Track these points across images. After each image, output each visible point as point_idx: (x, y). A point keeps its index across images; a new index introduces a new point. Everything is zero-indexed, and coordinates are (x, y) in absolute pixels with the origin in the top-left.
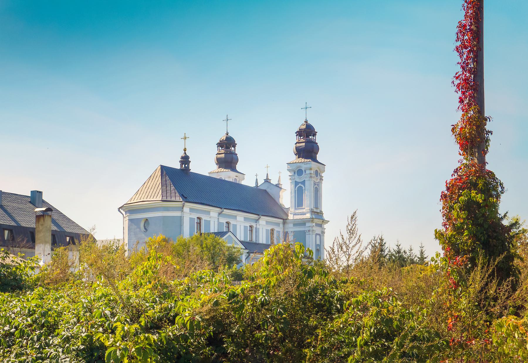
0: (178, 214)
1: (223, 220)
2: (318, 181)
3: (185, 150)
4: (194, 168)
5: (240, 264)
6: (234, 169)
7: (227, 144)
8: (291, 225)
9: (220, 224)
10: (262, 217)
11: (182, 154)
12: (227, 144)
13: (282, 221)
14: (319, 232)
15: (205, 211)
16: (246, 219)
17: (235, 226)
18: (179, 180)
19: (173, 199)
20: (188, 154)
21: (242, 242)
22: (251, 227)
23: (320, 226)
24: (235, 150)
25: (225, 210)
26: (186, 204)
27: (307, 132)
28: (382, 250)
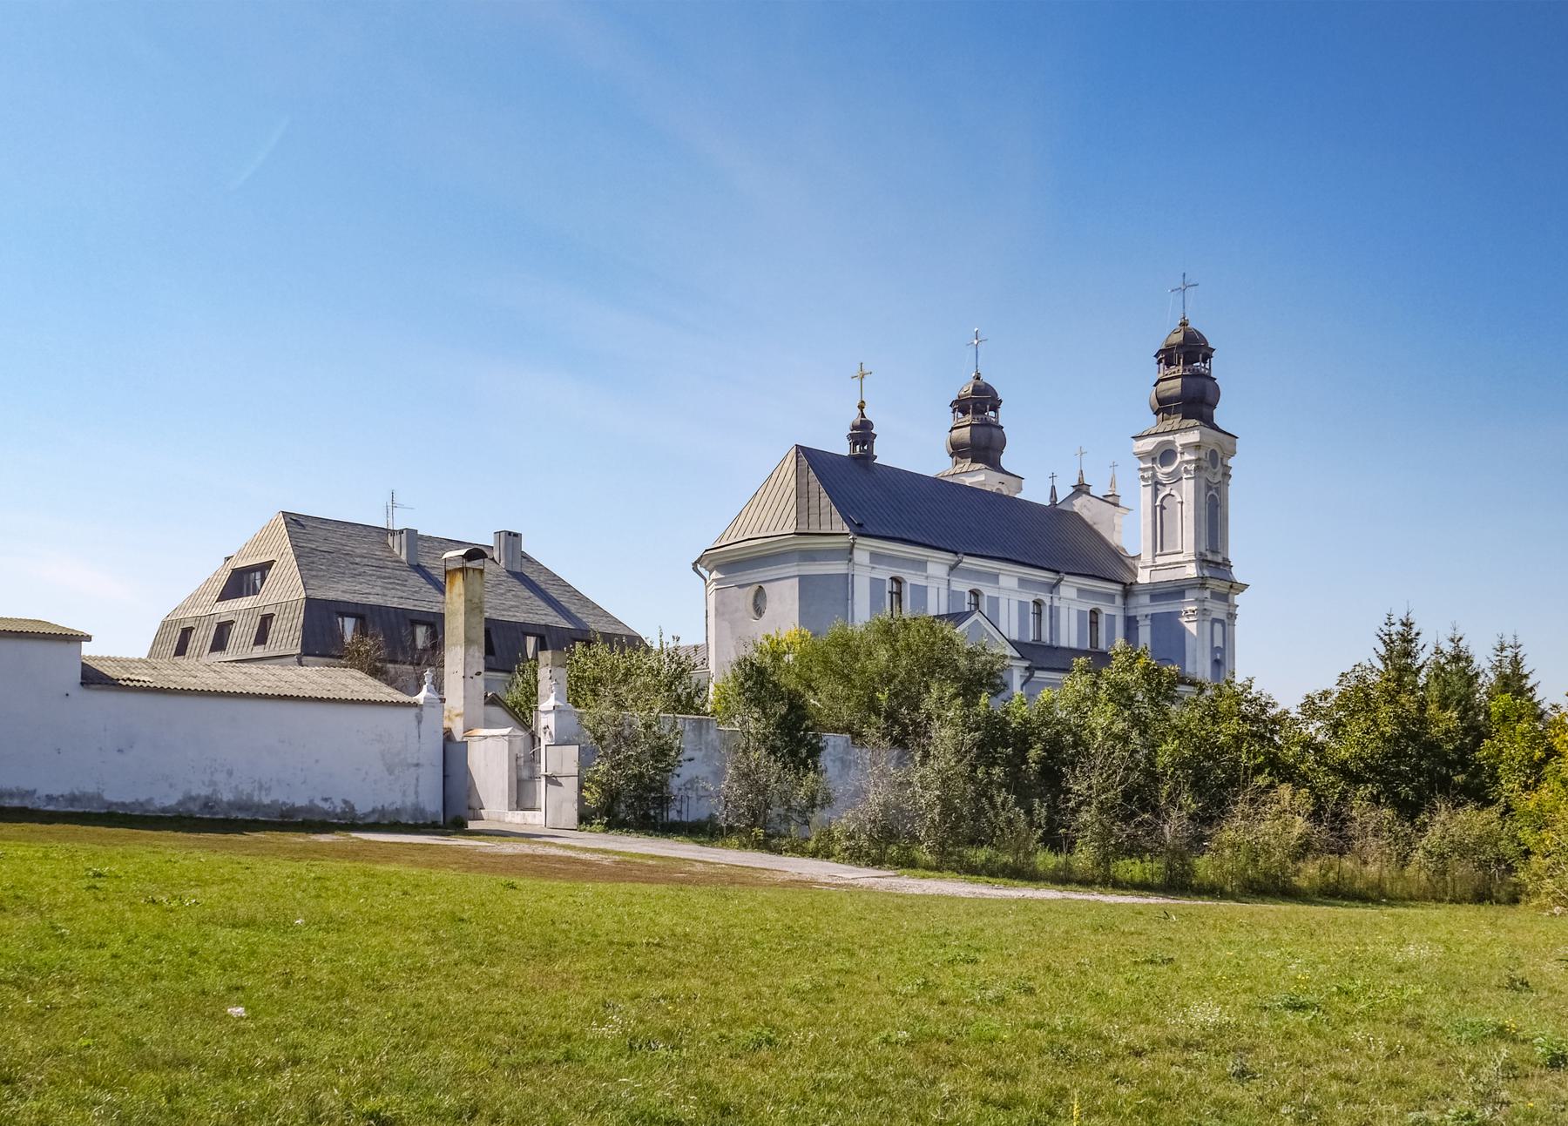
0: (838, 568)
1: (963, 586)
2: (1219, 478)
3: (861, 407)
4: (886, 453)
5: (1003, 696)
6: (995, 465)
7: (979, 403)
8: (1145, 599)
9: (952, 595)
10: (1067, 578)
11: (854, 416)
12: (979, 403)
13: (1119, 587)
14: (1222, 616)
15: (913, 561)
16: (1023, 582)
17: (994, 602)
18: (854, 487)
19: (825, 529)
20: (868, 417)
21: (1012, 643)
22: (1038, 603)
23: (1223, 597)
24: (997, 417)
25: (967, 559)
26: (859, 540)
27: (1189, 351)
28: (1407, 654)
